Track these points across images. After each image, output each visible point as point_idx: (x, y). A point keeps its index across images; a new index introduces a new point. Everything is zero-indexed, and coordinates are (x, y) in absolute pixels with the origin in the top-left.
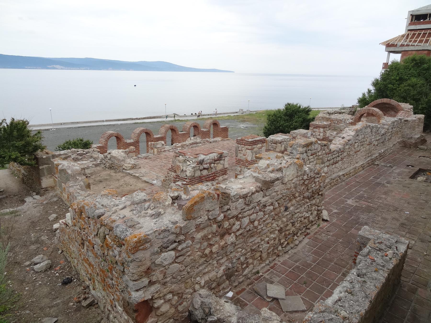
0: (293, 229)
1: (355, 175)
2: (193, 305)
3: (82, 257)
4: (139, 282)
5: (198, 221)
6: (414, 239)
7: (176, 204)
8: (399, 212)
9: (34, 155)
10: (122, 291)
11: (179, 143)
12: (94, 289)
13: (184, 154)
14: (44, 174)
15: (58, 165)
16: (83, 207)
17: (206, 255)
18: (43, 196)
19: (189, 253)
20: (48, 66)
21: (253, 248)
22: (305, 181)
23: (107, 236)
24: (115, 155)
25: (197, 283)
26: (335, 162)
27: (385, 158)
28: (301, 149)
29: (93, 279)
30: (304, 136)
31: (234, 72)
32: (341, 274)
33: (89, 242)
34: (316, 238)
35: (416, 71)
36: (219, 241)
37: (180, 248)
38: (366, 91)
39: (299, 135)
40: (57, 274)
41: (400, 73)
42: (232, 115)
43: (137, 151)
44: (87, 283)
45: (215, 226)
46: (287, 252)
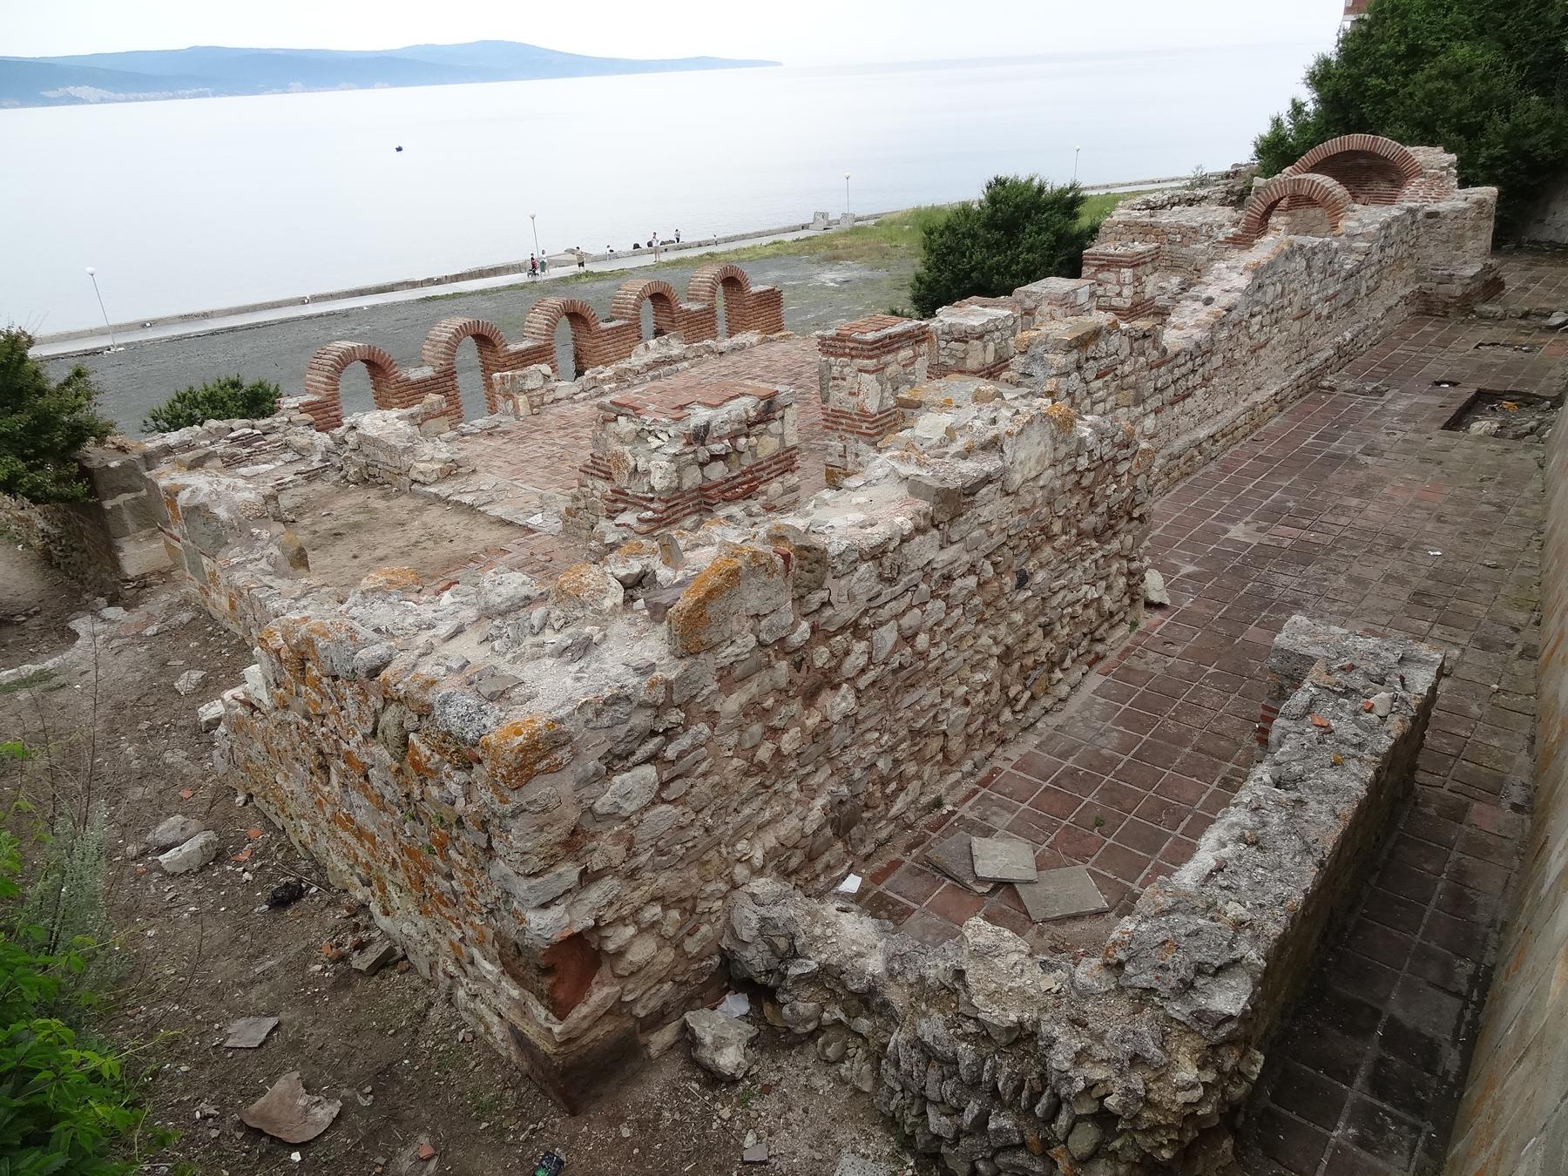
0: (1049, 645)
1: (1252, 432)
2: (734, 933)
3: (328, 810)
4: (547, 877)
5: (723, 655)
6: (1459, 641)
7: (640, 603)
8: (1406, 551)
9: (75, 461)
10: (491, 912)
11: (606, 364)
12: (387, 914)
13: (633, 411)
14: (125, 526)
15: (173, 493)
16: (309, 642)
17: (762, 767)
18: (136, 606)
19: (703, 767)
20: (44, 93)
21: (918, 725)
22: (1082, 474)
23: (411, 736)
24: (374, 433)
25: (739, 860)
26: (1180, 392)
27: (1359, 360)
28: (1059, 360)
29: (379, 879)
30: (1067, 304)
31: (780, 64)
32: (1216, 783)
33: (348, 758)
34: (1128, 669)
35: (1470, 14)
36: (802, 715)
37: (671, 752)
38: (1284, 109)
39: (1045, 303)
40: (246, 875)
41: (1409, 29)
42: (788, 238)
43: (454, 411)
44: (360, 896)
45: (783, 666)
46: (1032, 725)
